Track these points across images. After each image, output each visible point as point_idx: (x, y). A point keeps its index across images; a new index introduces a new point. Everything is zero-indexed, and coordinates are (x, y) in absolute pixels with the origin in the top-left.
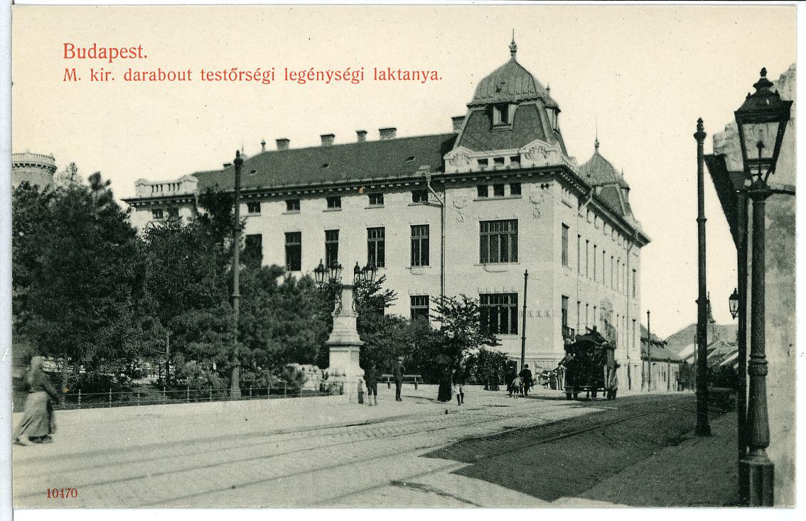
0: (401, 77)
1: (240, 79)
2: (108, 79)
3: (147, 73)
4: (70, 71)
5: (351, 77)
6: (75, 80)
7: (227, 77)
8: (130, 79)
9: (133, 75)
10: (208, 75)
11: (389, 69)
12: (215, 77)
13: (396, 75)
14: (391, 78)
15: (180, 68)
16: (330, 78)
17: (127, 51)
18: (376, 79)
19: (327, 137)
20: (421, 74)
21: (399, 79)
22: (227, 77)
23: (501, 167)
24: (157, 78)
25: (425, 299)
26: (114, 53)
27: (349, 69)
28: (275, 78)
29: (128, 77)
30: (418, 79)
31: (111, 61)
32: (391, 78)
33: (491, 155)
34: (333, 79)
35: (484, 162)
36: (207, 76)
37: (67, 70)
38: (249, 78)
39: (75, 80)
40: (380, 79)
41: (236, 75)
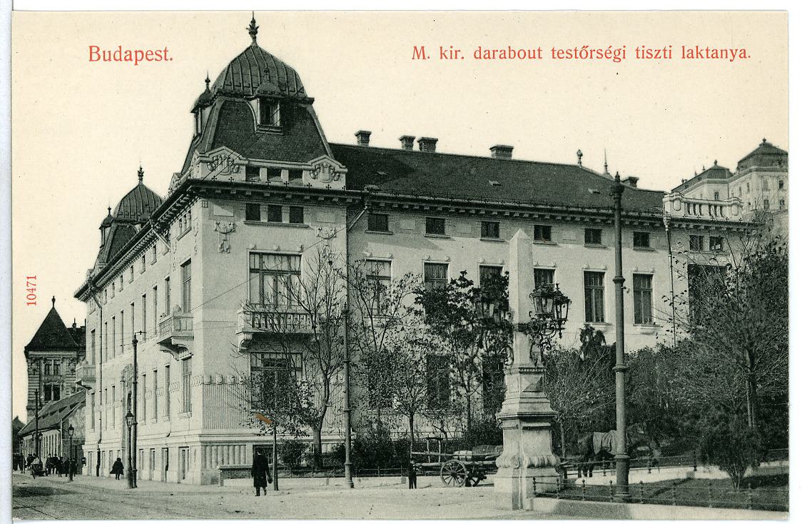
0: (710, 56)
1: (591, 57)
2: (496, 56)
3: (497, 51)
4: (419, 49)
5: (613, 55)
6: (424, 58)
7: (578, 55)
8: (480, 58)
9: (483, 54)
10: (606, 53)
11: (697, 47)
12: (565, 55)
13: (704, 53)
14: (699, 56)
15: (530, 46)
16: (734, 56)
17: (152, 54)
18: (684, 57)
19: (364, 136)
20: (729, 52)
21: (708, 57)
22: (578, 55)
23: (275, 182)
24: (507, 55)
25: (276, 355)
26: (139, 55)
27: (610, 47)
28: (672, 56)
29: (478, 55)
30: (727, 57)
31: (136, 64)
32: (699, 56)
33: (264, 165)
34: (737, 57)
35: (252, 171)
36: (557, 54)
37: (415, 48)
38: (600, 56)
39: (424, 58)
40: (688, 57)
41: (585, 53)
